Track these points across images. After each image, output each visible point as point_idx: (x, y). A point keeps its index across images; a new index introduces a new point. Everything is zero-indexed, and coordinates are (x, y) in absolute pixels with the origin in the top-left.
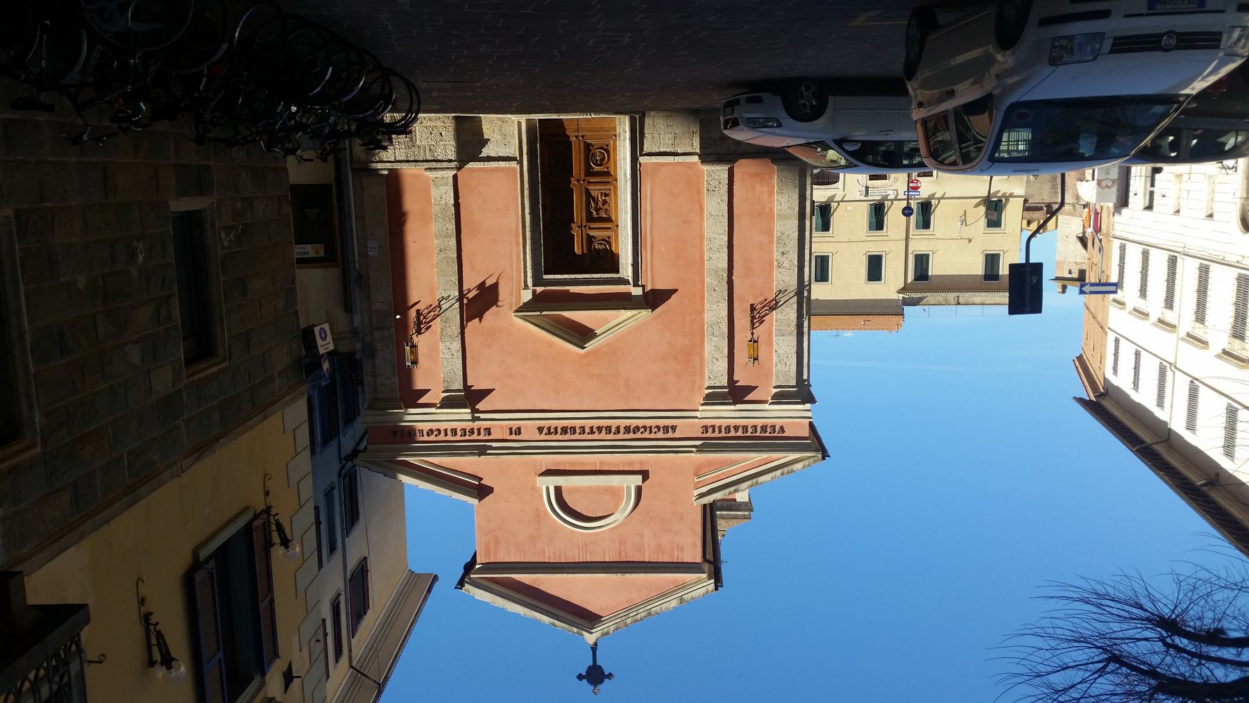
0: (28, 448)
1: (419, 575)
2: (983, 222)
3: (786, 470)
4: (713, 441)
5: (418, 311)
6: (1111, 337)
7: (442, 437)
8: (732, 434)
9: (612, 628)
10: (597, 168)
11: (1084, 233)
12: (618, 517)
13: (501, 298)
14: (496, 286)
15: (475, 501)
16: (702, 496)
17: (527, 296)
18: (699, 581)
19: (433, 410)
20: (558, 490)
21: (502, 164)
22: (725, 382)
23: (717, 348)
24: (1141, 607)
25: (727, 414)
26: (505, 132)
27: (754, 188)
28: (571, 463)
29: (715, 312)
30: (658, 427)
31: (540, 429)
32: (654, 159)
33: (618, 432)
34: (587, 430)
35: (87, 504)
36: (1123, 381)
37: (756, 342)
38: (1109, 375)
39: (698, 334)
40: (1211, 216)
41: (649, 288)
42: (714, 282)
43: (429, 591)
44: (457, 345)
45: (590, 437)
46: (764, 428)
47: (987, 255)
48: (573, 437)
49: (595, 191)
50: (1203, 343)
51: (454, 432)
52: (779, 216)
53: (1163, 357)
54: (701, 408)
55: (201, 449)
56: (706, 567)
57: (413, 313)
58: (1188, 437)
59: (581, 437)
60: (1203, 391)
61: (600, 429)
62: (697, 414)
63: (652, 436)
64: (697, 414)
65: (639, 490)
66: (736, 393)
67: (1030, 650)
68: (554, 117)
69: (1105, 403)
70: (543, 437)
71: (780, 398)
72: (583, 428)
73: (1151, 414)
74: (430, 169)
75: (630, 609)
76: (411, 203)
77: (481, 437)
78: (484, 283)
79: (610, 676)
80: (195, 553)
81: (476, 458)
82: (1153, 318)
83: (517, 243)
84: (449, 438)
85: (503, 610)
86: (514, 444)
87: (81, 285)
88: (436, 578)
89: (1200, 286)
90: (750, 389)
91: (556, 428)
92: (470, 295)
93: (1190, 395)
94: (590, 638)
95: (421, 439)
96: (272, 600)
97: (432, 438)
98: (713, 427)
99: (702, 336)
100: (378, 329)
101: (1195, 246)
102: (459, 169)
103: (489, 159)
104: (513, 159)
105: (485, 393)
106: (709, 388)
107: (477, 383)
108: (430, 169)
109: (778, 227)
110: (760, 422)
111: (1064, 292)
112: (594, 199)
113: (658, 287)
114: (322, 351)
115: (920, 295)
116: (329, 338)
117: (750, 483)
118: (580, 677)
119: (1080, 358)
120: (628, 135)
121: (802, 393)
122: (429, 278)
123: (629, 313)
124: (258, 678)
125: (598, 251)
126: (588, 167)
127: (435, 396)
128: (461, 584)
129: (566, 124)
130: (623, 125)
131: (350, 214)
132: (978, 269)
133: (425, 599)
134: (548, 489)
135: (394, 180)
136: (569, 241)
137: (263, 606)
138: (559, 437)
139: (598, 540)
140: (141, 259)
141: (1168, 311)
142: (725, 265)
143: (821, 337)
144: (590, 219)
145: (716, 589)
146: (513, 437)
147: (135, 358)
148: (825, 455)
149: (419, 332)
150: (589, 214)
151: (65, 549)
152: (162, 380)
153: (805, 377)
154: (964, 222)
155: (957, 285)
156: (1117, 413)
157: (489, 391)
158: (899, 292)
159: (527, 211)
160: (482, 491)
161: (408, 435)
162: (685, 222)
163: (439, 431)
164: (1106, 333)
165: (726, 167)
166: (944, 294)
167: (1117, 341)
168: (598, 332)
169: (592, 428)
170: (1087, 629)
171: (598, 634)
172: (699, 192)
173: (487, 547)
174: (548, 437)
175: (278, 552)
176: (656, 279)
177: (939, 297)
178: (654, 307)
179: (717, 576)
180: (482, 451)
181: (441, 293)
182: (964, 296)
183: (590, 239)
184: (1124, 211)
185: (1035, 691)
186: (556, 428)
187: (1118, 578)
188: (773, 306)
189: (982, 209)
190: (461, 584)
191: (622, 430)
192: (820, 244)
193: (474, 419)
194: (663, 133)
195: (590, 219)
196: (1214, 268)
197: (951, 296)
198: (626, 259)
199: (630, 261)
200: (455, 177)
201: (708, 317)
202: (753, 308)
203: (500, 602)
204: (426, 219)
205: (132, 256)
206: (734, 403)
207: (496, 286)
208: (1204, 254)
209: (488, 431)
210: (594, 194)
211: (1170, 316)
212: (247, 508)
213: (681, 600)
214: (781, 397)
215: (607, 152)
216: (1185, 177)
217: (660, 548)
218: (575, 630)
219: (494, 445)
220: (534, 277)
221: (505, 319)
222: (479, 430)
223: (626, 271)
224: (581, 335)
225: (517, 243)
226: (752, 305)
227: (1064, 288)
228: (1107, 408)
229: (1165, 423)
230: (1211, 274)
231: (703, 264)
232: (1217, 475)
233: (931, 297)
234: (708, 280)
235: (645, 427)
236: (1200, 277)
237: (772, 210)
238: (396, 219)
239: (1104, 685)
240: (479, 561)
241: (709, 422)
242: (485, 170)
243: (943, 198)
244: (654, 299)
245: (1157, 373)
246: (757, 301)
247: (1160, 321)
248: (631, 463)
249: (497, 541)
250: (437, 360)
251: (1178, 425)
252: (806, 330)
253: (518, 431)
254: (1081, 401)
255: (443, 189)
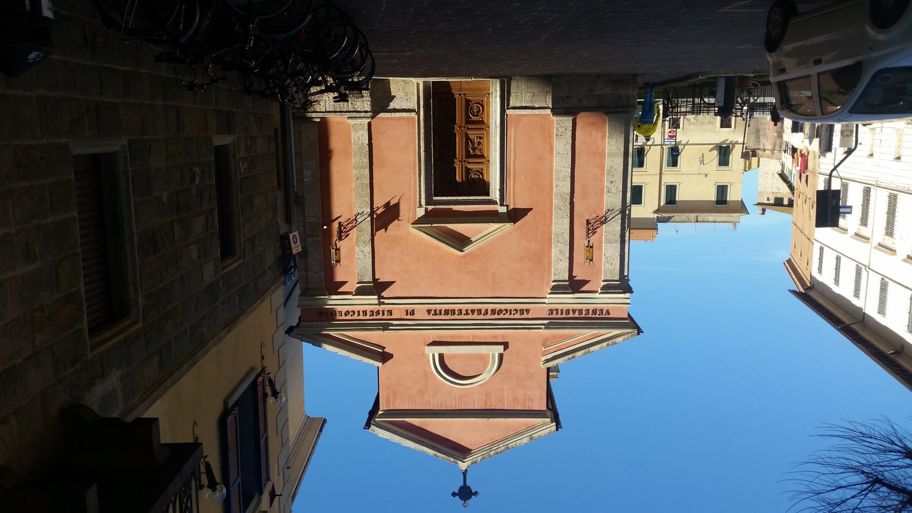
0: (134, 323)
1: (313, 419)
2: (716, 161)
3: (610, 342)
4: (557, 320)
5: (340, 223)
6: (817, 247)
7: (355, 317)
8: (571, 315)
9: (479, 458)
10: (474, 118)
11: (783, 171)
12: (485, 377)
13: (401, 214)
14: (397, 205)
15: (380, 364)
16: (547, 361)
17: (421, 212)
18: (544, 424)
19: (350, 297)
20: (441, 356)
21: (405, 114)
22: (566, 277)
23: (561, 252)
24: (893, 443)
25: (568, 300)
26: (407, 91)
27: (591, 133)
28: (451, 337)
29: (560, 225)
30: (516, 310)
31: (429, 311)
32: (517, 112)
33: (487, 313)
34: (464, 312)
35: (170, 366)
36: (826, 278)
37: (591, 247)
38: (815, 274)
39: (547, 241)
40: (898, 158)
41: (511, 207)
42: (560, 204)
43: (321, 431)
44: (369, 248)
45: (466, 317)
46: (594, 311)
47: (719, 187)
48: (453, 317)
49: (473, 135)
50: (893, 251)
51: (365, 313)
52: (609, 154)
53: (840, 259)
54: (548, 296)
55: (230, 323)
56: (549, 413)
57: (335, 225)
58: (879, 319)
59: (459, 317)
60: (891, 285)
61: (473, 311)
62: (546, 301)
63: (512, 316)
64: (546, 301)
65: (501, 356)
66: (574, 285)
67: (816, 475)
68: (444, 80)
69: (812, 294)
70: (431, 317)
71: (607, 289)
72: (460, 310)
73: (849, 302)
74: (351, 118)
75: (492, 444)
76: (335, 143)
77: (384, 317)
78: (389, 203)
79: (476, 493)
80: (226, 402)
81: (380, 332)
82: (851, 232)
83: (415, 174)
84: (361, 317)
85: (399, 445)
86: (409, 322)
87: (165, 199)
88: (325, 421)
89: (889, 209)
90: (585, 282)
91: (440, 311)
92: (379, 212)
93: (881, 289)
94: (463, 466)
95: (340, 318)
96: (267, 437)
97: (349, 317)
98: (557, 310)
99: (550, 243)
100: (310, 236)
101: (885, 180)
102: (373, 118)
103: (395, 111)
104: (413, 111)
105: (389, 284)
106: (554, 281)
107: (383, 277)
108: (351, 118)
109: (608, 162)
110: (591, 307)
111: (763, 213)
112: (471, 141)
113: (518, 206)
114: (294, 252)
115: (669, 215)
116: (299, 243)
117: (583, 351)
118: (454, 494)
119: (789, 261)
120: (498, 93)
121: (623, 285)
122: (349, 198)
123: (496, 226)
124: (256, 496)
125: (474, 180)
126: (468, 117)
127: (352, 286)
128: (368, 425)
129: (452, 85)
130: (495, 88)
131: (291, 151)
132: (712, 196)
133: (318, 436)
134: (434, 355)
135: (323, 127)
136: (452, 172)
137: (262, 441)
138: (442, 317)
139: (470, 394)
140: (197, 182)
141: (864, 228)
142: (569, 191)
143: (637, 245)
144: (468, 155)
145: (557, 430)
146: (409, 317)
147: (194, 255)
148: (640, 331)
149: (340, 239)
150: (468, 152)
151: (154, 403)
152: (209, 272)
153: (626, 274)
154: (702, 162)
155: (696, 208)
156: (821, 301)
157: (392, 283)
158: (655, 212)
159: (422, 149)
160: (385, 357)
161: (330, 315)
162: (539, 158)
163: (354, 312)
164: (813, 243)
165: (571, 118)
166: (687, 215)
167: (821, 249)
168: (473, 239)
169: (467, 310)
170: (856, 459)
171: (469, 463)
172: (550, 136)
173: (388, 398)
174: (435, 317)
175: (271, 400)
176: (516, 201)
177: (684, 216)
178: (515, 221)
179: (556, 419)
180: (385, 327)
181: (357, 210)
182: (702, 216)
183: (468, 171)
184: (828, 154)
185: (815, 504)
186: (440, 311)
187: (874, 422)
188: (603, 221)
189: (715, 153)
190: (368, 425)
191: (489, 312)
192: (637, 177)
193: (380, 304)
194: (521, 94)
195: (468, 155)
196: (901, 197)
197: (692, 216)
198: (495, 186)
199: (498, 187)
200: (369, 124)
201: (554, 229)
202: (588, 222)
203: (396, 439)
204: (347, 155)
205: (193, 179)
206: (573, 293)
207: (397, 205)
208: (893, 186)
209: (390, 312)
210: (472, 137)
211: (864, 231)
212: (253, 369)
213: (531, 438)
214: (608, 288)
215: (482, 106)
216: (878, 130)
217: (515, 400)
218: (452, 459)
219: (395, 322)
220: (426, 198)
221: (404, 229)
222: (383, 311)
223: (495, 194)
224: (461, 242)
225: (415, 174)
226: (587, 220)
227: (764, 211)
228: (814, 297)
229: (861, 309)
230: (898, 201)
231: (552, 189)
232: (902, 346)
233: (677, 216)
234: (555, 202)
235: (506, 310)
236: (890, 203)
237: (604, 150)
238: (325, 155)
239: (870, 501)
240: (381, 408)
241: (554, 307)
242: (392, 118)
243: (687, 144)
244: (515, 215)
245: (854, 272)
246: (591, 217)
247: (856, 234)
248: (495, 337)
249: (395, 393)
250: (353, 260)
251: (871, 310)
252: (627, 239)
253: (413, 313)
254: (794, 292)
255: (360, 133)
